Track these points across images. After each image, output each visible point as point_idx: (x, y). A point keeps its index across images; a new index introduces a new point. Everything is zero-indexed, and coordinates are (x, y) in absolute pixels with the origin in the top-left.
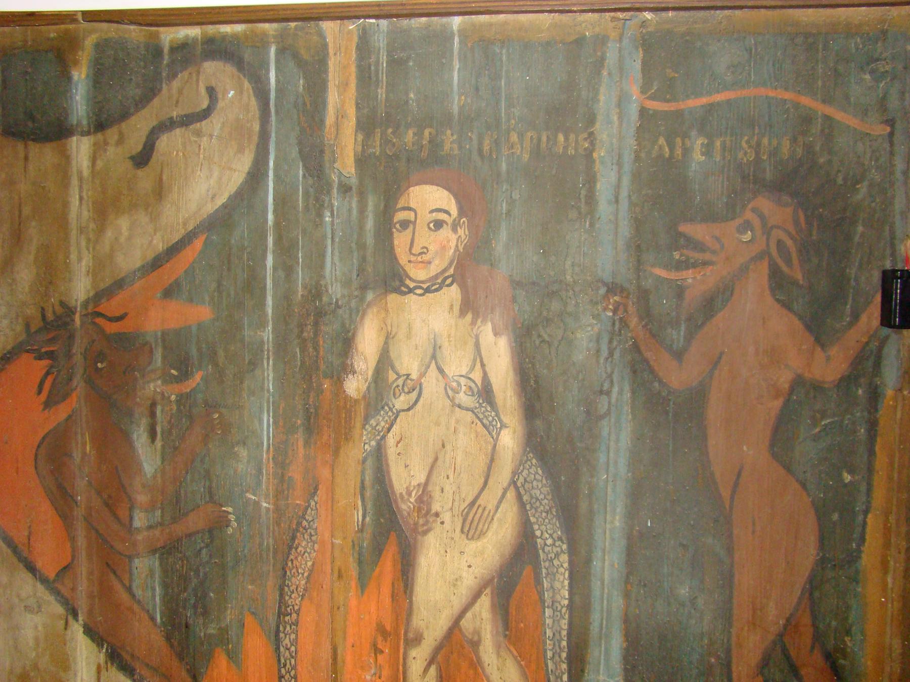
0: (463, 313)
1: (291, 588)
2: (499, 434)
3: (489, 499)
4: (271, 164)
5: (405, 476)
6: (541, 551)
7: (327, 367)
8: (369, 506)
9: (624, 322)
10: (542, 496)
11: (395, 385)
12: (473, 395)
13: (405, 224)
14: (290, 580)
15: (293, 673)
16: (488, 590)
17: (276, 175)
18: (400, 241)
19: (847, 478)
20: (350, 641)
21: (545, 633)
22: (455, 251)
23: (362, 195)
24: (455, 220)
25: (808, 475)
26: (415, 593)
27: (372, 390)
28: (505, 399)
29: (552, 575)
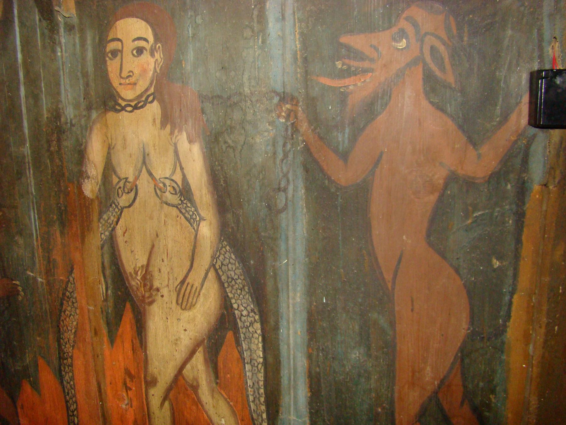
0: (163, 125)
1: (65, 341)
2: (199, 225)
3: (195, 278)
4: (16, 12)
5: (133, 259)
6: (238, 320)
7: (70, 174)
8: (109, 282)
9: (295, 128)
10: (236, 277)
11: (118, 187)
12: (176, 194)
13: (115, 53)
14: (63, 334)
15: (74, 399)
16: (201, 349)
17: (21, 22)
18: (112, 66)
19: (496, 263)
20: (108, 380)
21: (247, 382)
22: (153, 74)
23: (82, 31)
24: (152, 46)
25: (461, 260)
26: (148, 348)
27: (102, 191)
28: (201, 197)
29: (249, 339)
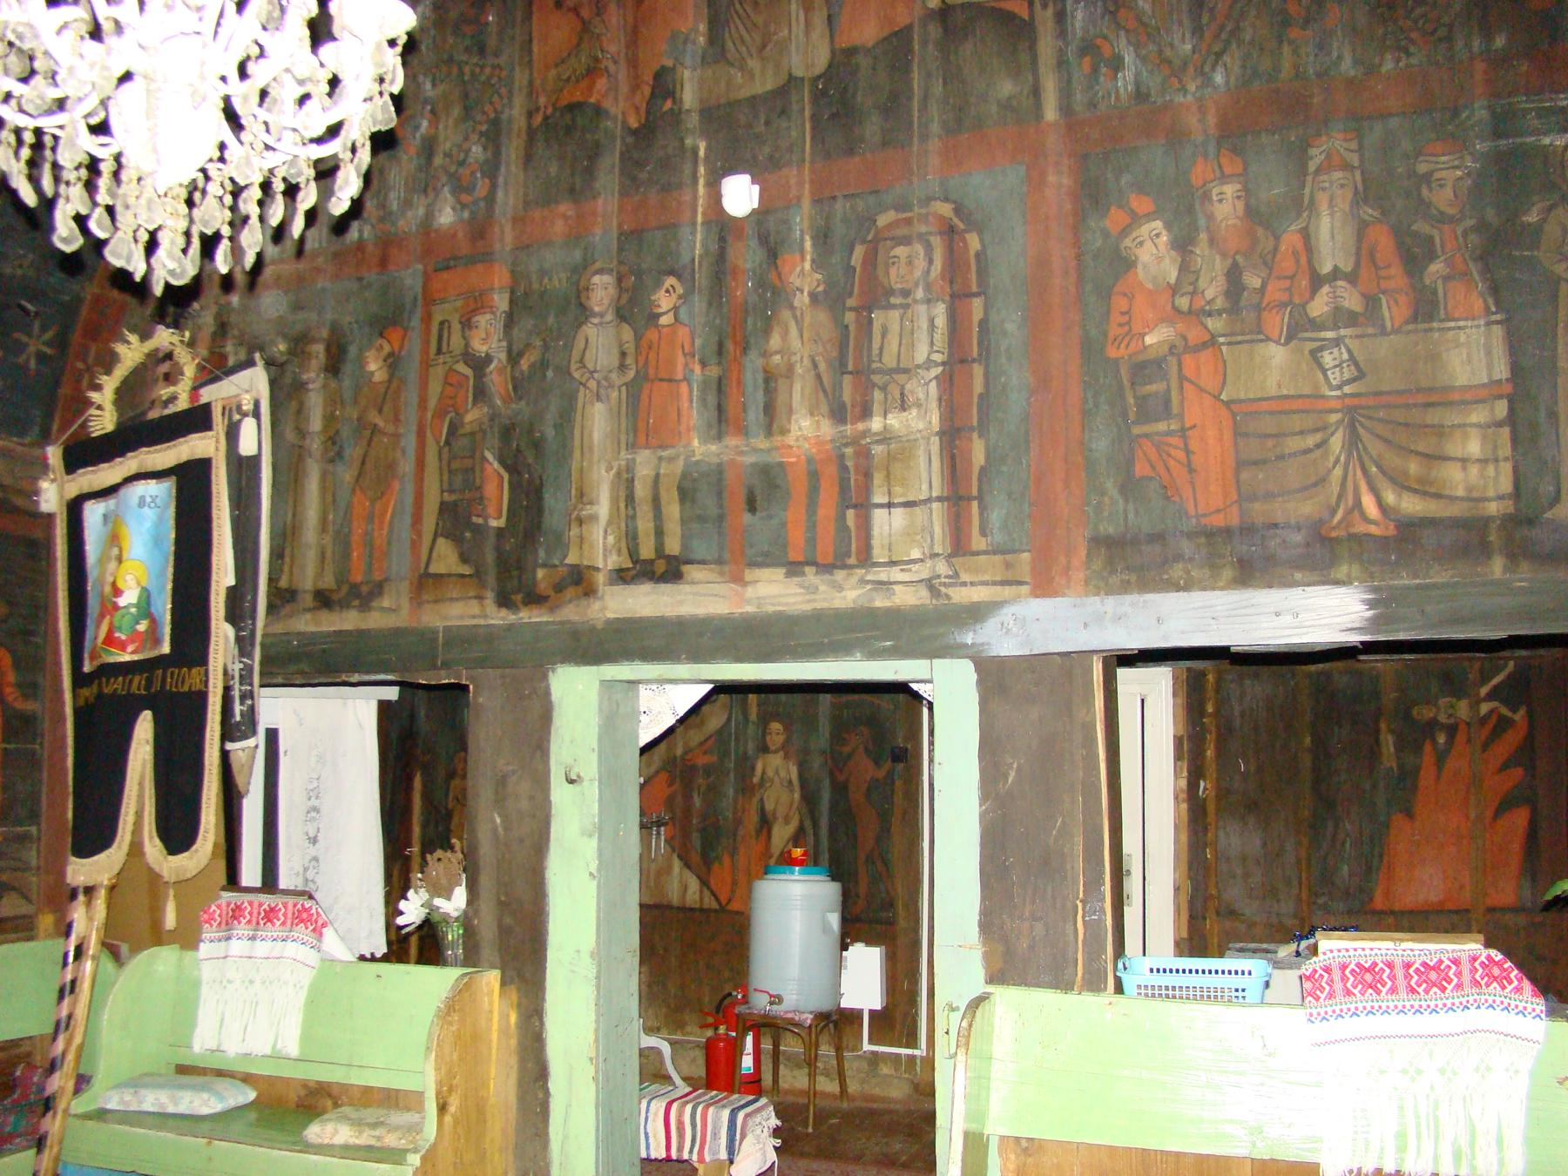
5: (769, 806)
